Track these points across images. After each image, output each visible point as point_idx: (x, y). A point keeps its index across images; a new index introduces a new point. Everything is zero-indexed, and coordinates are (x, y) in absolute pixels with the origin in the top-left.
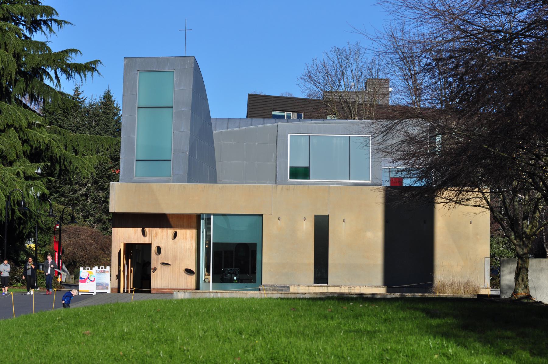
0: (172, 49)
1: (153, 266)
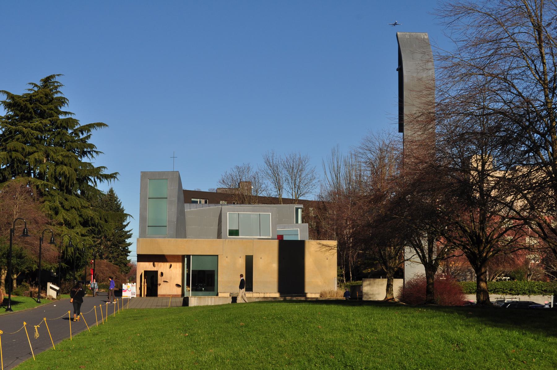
0: (168, 168)
1: (159, 283)
